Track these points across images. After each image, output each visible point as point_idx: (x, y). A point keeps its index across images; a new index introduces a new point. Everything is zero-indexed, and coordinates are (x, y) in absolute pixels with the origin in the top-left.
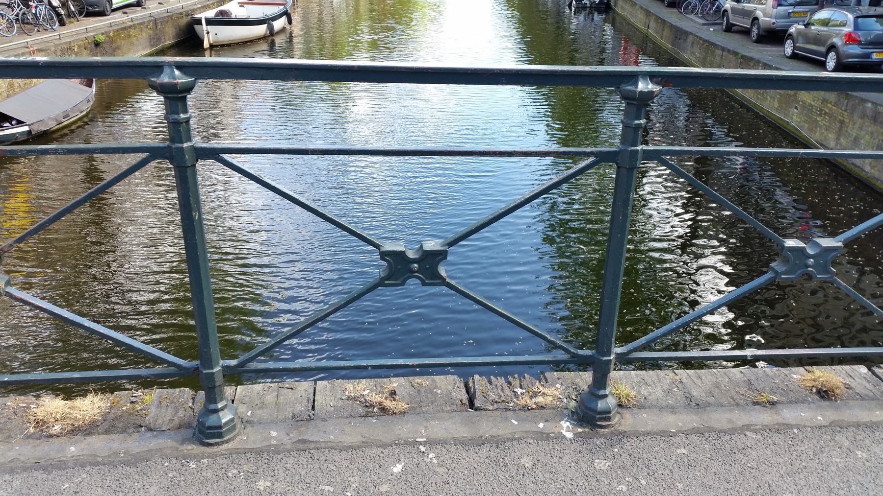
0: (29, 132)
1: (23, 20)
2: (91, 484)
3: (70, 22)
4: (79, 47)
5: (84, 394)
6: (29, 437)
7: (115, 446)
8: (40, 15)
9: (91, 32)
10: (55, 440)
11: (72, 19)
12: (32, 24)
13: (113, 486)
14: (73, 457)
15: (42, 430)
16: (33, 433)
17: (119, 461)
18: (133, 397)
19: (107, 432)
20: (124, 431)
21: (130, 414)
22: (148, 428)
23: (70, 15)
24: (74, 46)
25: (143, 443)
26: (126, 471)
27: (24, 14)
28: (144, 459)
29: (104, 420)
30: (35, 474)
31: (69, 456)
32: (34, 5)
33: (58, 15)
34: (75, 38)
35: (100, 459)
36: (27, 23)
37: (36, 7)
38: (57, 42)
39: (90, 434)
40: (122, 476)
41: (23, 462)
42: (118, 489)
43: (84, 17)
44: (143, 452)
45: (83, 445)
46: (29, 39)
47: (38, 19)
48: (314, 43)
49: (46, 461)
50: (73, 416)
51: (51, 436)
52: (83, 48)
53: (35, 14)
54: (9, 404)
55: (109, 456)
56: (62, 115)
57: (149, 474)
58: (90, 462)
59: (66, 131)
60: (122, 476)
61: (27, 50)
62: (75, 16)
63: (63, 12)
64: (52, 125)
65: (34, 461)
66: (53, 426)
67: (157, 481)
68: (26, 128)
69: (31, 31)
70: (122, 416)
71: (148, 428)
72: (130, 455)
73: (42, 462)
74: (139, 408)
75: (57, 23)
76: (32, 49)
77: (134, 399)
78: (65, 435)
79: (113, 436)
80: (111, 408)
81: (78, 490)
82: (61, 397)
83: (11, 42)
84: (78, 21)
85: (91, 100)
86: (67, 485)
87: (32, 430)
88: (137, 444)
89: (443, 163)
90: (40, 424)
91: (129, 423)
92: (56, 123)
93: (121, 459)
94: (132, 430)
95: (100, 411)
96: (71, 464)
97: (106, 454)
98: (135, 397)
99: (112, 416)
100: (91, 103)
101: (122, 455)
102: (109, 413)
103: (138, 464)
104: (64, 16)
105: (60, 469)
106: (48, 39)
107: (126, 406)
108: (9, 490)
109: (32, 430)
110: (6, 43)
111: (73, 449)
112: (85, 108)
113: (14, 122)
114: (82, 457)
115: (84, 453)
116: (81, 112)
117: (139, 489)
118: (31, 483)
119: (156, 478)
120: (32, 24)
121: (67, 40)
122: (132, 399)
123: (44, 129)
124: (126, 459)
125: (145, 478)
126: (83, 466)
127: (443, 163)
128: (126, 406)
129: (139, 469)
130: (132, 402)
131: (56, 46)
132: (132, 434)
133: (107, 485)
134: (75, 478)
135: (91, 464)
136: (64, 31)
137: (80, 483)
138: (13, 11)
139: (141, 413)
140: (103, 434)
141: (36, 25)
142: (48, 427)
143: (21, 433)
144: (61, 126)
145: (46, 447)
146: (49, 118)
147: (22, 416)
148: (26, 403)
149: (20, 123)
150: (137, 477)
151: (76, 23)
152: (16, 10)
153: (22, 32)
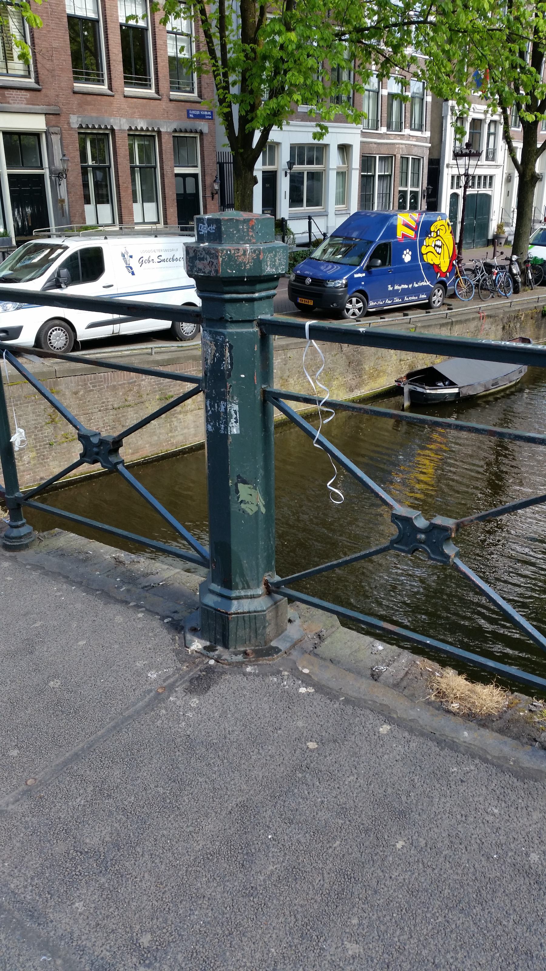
0: (458, 394)
1: (482, 285)
2: (477, 779)
3: (524, 290)
4: (526, 316)
5: (486, 681)
6: (429, 703)
7: (506, 750)
8: (499, 281)
9: (542, 301)
10: (451, 717)
11: (527, 288)
12: (489, 290)
13: (498, 792)
14: (465, 742)
15: (442, 702)
16: (434, 702)
17: (508, 768)
18: (532, 704)
19: (500, 731)
20: (517, 738)
21: (527, 723)
22: (542, 746)
23: (524, 284)
24: (522, 315)
25: (534, 759)
26: (513, 782)
27: (485, 280)
28: (532, 778)
29: (500, 718)
30: (430, 743)
31: (462, 740)
32: (496, 271)
33: (515, 282)
34: (525, 306)
35: (490, 758)
36: (485, 289)
37: (497, 274)
38: (507, 310)
39: (484, 726)
40: (508, 786)
41: (421, 726)
42: (501, 797)
43: (539, 285)
44: (533, 769)
45: (476, 735)
46: (483, 305)
47: (495, 285)
48: (453, 82)
49: (440, 735)
50: (473, 700)
51: (448, 712)
52: (529, 318)
53: (495, 281)
54: (418, 663)
55: (499, 758)
56: (491, 382)
57: (535, 797)
58: (480, 756)
59: (491, 399)
60: (508, 786)
61: (478, 315)
62: (530, 284)
63: (520, 280)
64: (479, 390)
65: (431, 730)
66: (452, 703)
67: (542, 808)
68: (456, 390)
69: (486, 297)
70: (518, 721)
71: (542, 746)
72: (520, 767)
73: (437, 733)
74: (537, 720)
75: (512, 290)
76: (482, 314)
77: (534, 709)
78: (461, 717)
79: (506, 739)
80: (508, 707)
81: (464, 780)
82: (464, 676)
83: (466, 306)
84: (532, 289)
85: (523, 371)
86: (455, 769)
87: (433, 698)
88: (529, 758)
89: (474, 465)
90: (441, 694)
91: (524, 732)
92: (484, 389)
93: (510, 767)
94: (525, 740)
95: (498, 706)
96: (462, 749)
97: (496, 755)
98: (535, 706)
99: (507, 716)
100: (522, 374)
101: (512, 763)
102: (505, 712)
103: (526, 781)
104: (520, 284)
105: (452, 749)
106: (500, 306)
107: (524, 711)
108: (406, 748)
109: (433, 698)
110: (462, 307)
111: (466, 734)
112: (515, 378)
113: (447, 383)
114: (473, 747)
115: (476, 743)
116: (511, 382)
117: (522, 808)
118: (425, 751)
119: (542, 804)
120: (489, 290)
121: (517, 308)
122: (531, 706)
123: (472, 393)
124: (515, 769)
125: (530, 798)
126: (473, 756)
127: (474, 465)
128: (524, 711)
129: (526, 786)
130: (530, 711)
131: (505, 313)
132: (525, 746)
133: (492, 788)
134: (463, 766)
135: (480, 758)
136: (517, 299)
137: (468, 773)
138: (475, 276)
139: (537, 725)
140: (497, 732)
141: (493, 291)
142: (447, 701)
143: (424, 697)
144: (488, 392)
145: (443, 722)
146: (479, 384)
147: (427, 680)
148: (432, 668)
149: (452, 384)
150: (523, 794)
151: (529, 291)
152: (479, 276)
153: (479, 298)
